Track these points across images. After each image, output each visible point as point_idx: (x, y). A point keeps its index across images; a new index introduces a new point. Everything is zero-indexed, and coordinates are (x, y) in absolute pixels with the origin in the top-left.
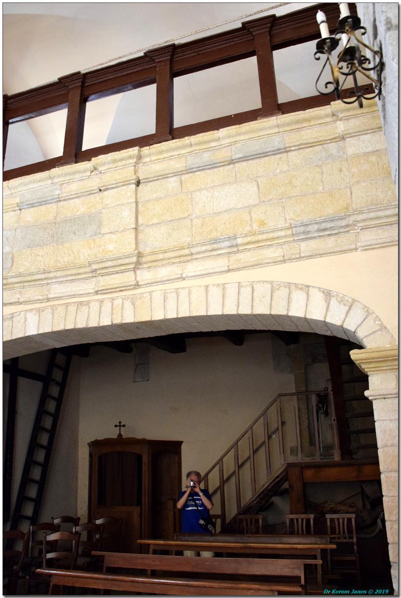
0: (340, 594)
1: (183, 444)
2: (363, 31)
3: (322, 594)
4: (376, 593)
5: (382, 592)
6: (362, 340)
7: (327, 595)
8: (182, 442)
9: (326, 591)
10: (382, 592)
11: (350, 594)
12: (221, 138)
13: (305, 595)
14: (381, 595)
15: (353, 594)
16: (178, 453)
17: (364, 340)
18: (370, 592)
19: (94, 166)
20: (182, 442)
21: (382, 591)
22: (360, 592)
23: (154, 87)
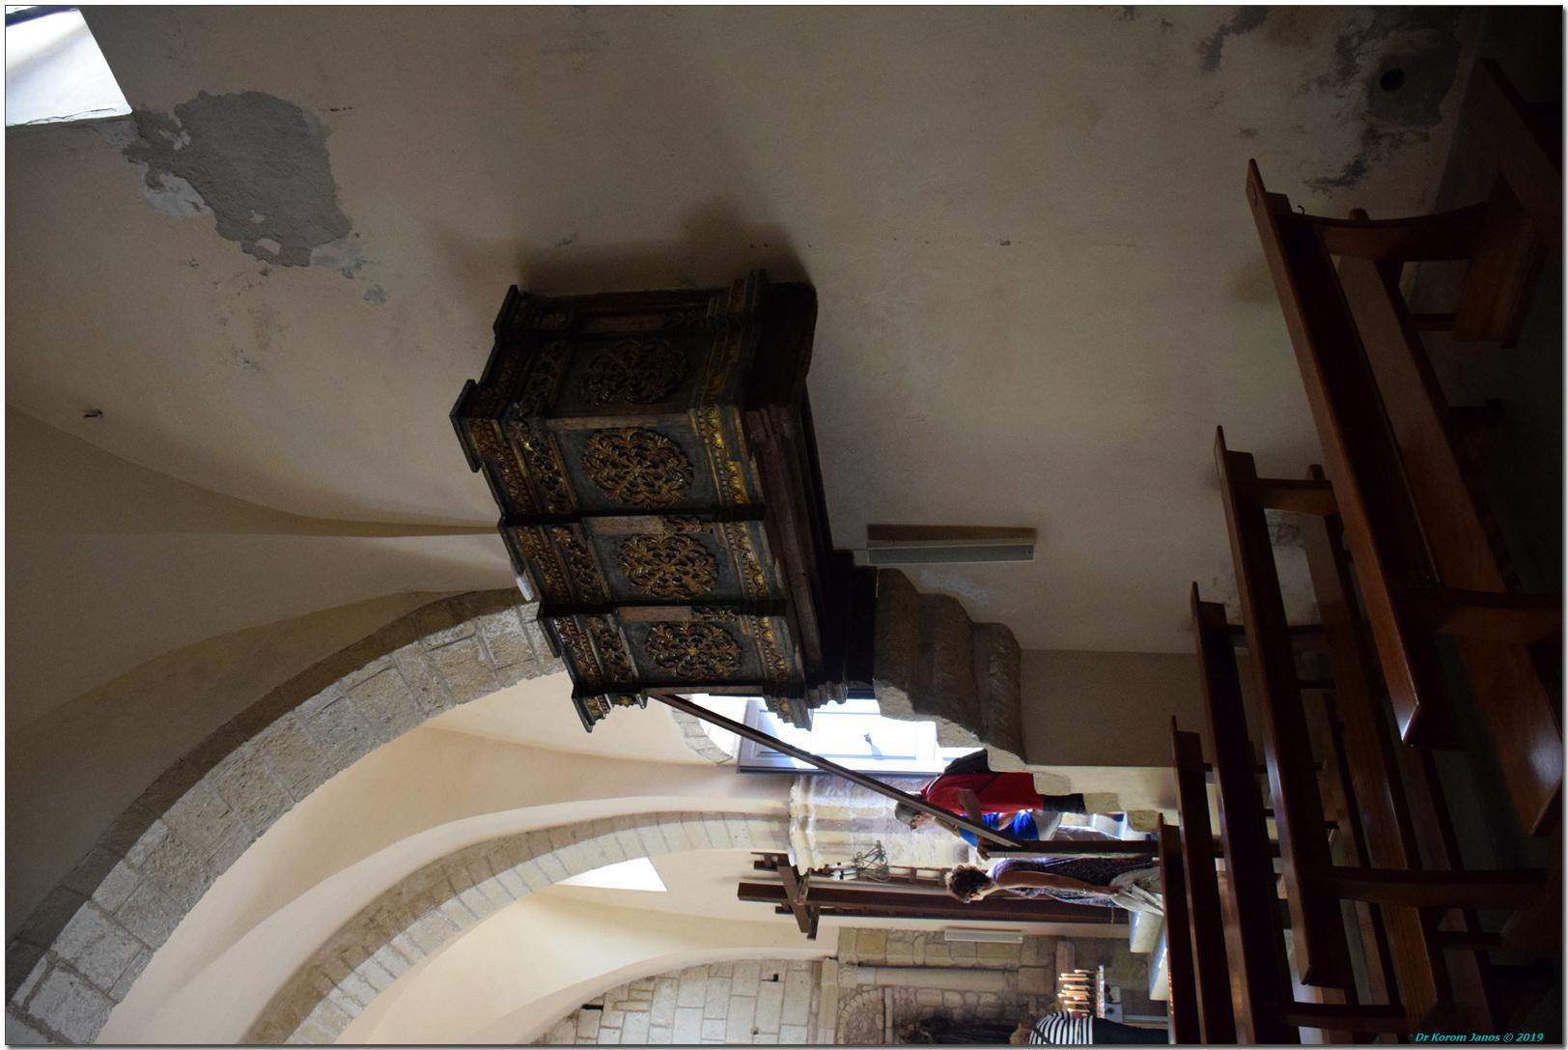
0: (1449, 1043)
1: (805, 730)
4: (1518, 1040)
5: (1531, 1038)
6: (943, 1004)
7: (1422, 1043)
8: (809, 730)
10: (1531, 1038)
11: (1468, 1043)
12: (167, 932)
13: (935, 1043)
14: (1529, 1043)
15: (1474, 1043)
16: (1546, 1042)
18: (1506, 1038)
20: (809, 730)
21: (1531, 1037)
22: (1486, 1038)
23: (1301, 1029)
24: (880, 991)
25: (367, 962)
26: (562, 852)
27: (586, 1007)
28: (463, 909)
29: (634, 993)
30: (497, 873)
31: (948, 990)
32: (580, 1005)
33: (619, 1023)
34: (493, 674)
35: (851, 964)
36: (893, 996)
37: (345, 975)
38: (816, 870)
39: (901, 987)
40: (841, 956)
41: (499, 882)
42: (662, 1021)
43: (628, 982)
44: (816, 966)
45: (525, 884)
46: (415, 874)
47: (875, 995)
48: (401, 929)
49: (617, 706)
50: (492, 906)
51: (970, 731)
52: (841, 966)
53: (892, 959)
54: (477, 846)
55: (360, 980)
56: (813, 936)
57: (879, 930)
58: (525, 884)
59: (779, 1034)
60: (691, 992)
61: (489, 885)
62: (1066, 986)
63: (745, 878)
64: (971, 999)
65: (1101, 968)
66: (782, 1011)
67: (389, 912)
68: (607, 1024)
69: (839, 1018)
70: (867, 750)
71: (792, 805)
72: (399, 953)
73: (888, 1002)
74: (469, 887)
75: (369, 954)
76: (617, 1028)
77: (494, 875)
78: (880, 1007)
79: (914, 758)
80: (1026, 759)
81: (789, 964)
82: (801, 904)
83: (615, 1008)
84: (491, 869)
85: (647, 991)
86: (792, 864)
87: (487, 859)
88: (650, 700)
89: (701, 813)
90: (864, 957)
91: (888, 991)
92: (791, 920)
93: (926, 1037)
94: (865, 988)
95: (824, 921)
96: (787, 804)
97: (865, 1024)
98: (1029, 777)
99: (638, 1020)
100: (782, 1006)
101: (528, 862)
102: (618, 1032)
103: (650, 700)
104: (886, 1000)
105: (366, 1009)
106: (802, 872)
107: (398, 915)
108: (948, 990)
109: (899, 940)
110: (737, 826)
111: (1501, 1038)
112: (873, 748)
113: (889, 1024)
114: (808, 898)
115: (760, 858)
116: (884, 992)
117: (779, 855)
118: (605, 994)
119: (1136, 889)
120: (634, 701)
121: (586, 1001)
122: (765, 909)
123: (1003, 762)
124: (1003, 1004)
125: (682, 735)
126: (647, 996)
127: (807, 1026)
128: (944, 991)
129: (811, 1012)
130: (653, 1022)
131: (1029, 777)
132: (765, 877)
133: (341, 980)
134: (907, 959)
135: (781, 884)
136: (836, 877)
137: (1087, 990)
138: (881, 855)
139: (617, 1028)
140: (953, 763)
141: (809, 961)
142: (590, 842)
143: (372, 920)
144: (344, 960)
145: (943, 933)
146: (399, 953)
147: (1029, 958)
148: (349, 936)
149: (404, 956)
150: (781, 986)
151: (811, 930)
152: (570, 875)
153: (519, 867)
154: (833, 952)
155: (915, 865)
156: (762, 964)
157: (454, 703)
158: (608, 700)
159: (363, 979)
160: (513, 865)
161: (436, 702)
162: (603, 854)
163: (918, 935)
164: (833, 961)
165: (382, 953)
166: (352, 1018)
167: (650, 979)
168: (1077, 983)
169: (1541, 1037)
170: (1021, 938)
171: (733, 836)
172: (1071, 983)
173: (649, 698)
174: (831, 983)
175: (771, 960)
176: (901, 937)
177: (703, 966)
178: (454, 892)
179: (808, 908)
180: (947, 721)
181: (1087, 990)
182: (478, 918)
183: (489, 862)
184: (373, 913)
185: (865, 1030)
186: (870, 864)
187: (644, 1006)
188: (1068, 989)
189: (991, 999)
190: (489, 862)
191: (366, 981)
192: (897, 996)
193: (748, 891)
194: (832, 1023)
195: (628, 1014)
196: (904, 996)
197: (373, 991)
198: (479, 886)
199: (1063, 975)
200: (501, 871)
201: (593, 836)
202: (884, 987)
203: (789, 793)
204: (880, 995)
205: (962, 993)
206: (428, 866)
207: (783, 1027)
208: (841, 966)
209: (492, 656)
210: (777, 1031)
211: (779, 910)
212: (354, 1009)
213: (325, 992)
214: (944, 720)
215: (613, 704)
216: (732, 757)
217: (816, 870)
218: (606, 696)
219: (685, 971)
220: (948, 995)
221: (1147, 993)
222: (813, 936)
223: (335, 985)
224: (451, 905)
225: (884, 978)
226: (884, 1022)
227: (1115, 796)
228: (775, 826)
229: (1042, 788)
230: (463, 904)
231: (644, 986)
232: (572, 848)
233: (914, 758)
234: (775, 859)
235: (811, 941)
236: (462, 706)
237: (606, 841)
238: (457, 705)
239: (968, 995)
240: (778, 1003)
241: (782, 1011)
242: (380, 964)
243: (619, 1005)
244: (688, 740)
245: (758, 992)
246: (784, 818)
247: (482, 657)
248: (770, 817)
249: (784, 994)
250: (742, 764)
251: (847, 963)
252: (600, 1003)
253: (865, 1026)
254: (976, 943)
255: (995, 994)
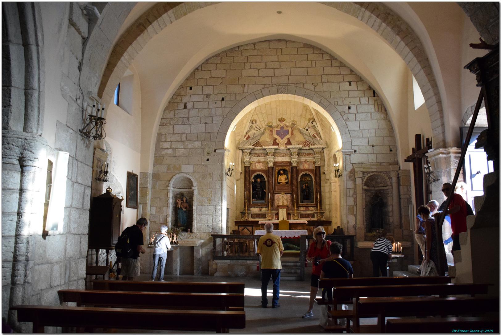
0: (463, 333)
2: (30, 284)
3: (228, 332)
7: (454, 333)
9: (454, 331)
11: (469, 333)
14: (488, 333)
15: (471, 333)
16: (494, 332)
17: (333, 218)
18: (481, 331)
19: (241, 212)
22: (475, 331)
24: (390, 185)
25: (375, 17)
26: (422, 72)
27: (374, 92)
28: (398, 43)
29: (380, 106)
30: (412, 52)
31: (393, 206)
32: (374, 90)
33: (370, 103)
34: (485, 27)
35: (398, 174)
36: (389, 189)
37: (369, 11)
38: (428, 159)
39: (392, 191)
40: (401, 171)
41: (409, 53)
42: (373, 116)
43: (384, 103)
44: (397, 163)
45: (409, 62)
46: (407, 24)
47: (389, 183)
48: (387, 25)
49: (476, 75)
50: (400, 53)
51: (481, 208)
52: (397, 171)
53: (401, 188)
54: (420, 42)
55: (369, 16)
56: (406, 161)
57: (410, 183)
58: (409, 62)
59: (373, 154)
60: (383, 124)
61: (407, 49)
62: (396, 245)
63: (423, 136)
64: (391, 214)
65: (403, 256)
66: (381, 154)
67: (393, 19)
68: (370, 99)
69: (380, 172)
70: (474, 172)
71: (450, 148)
72: (380, 26)
73: (387, 188)
74: (405, 43)
75: (378, 17)
76: (369, 103)
77: (411, 50)
78: (385, 185)
79: (472, 190)
80: (472, 229)
81: (396, 154)
82: (416, 156)
83: (375, 101)
84: (412, 49)
85: (382, 110)
86: (429, 151)
87: (416, 46)
88: (480, 88)
89: (443, 117)
90: (401, 179)
91: (390, 187)
92: (411, 153)
93: (377, 200)
94: (391, 180)
95: (411, 165)
96: (450, 146)
97: (379, 181)
98: (465, 230)
99: (372, 109)
100: (382, 154)
101: (417, 61)
102: (367, 103)
103: (480, 88)
104: (388, 187)
105: (361, 21)
106: (426, 155)
107: (392, 22)
108: (393, 206)
109: (408, 189)
110: (440, 130)
111: (480, 331)
112: (475, 175)
113: (380, 188)
114: (418, 158)
115: (430, 140)
116: (390, 186)
117: (432, 146)
118: (379, 96)
119: (429, 269)
120: (478, 81)
121: (376, 91)
122: (412, 144)
123: (470, 222)
124: (390, 224)
125: (472, 105)
126: (380, 110)
127: (377, 162)
128: (392, 205)
129: (381, 163)
130: (372, 113)
131: (465, 230)
132: (424, 144)
133: (368, 10)
134: (402, 193)
135: (422, 148)
136: (425, 166)
137: (396, 251)
138: (435, 181)
139: (369, 103)
140: (466, 201)
141: (398, 161)
142: (427, 81)
143: (389, 14)
144: (374, 9)
145: (411, 204)
146: (380, 26)
147: (405, 232)
148: (382, 8)
149: (379, 28)
150: (389, 153)
151: (408, 160)
152: (415, 76)
153: (415, 58)
154: (401, 168)
155: (432, 193)
156: (395, 146)
157: (470, 16)
158: (478, 72)
159: (370, 17)
160: (415, 56)
161: (470, 9)
162: (424, 86)
163: (410, 195)
164: (398, 169)
165: (379, 20)
166: (357, 18)
167: (386, 110)
168: (398, 248)
169: (492, 331)
170: (412, 230)
171: (436, 129)
172: (398, 246)
173: (481, 87)
174: (391, 169)
175: (397, 149)
176: (409, 190)
177: (392, 126)
178: (403, 39)
179: (415, 158)
180: (485, 200)
181: (396, 251)
182: (395, 49)
183: (415, 48)
184: (391, 14)
185: (378, 181)
186: (432, 178)
187: (377, 110)
188: (395, 245)
189: (391, 220)
190: (415, 48)
191: (369, 18)
192: (389, 190)
193: (418, 137)
194: (380, 170)
195: (373, 105)
196: (390, 193)
197: (366, 22)
198: (406, 47)
199: (400, 244)
200: (413, 53)
201: (429, 81)
202: (392, 186)
203: (454, 147)
204: (389, 185)
205: (392, 211)
206: (410, 27)
207: (375, 155)
208: (397, 171)
209: (492, 24)
210: (374, 153)
211: (413, 149)
212: (360, 18)
213: (363, 6)
214: (485, 198)
215: (477, 74)
216: (465, 125)
217: (428, 159)
218: (480, 71)
219: (390, 121)
220: (391, 206)
221: (394, 270)
222: (406, 161)
223: (366, 9)
224: (398, 38)
225: (395, 185)
226: (380, 187)
227: (461, 261)
228: (441, 144)
229: (461, 235)
230: (400, 42)
231: (383, 109)
232: (424, 75)
233: (472, 190)
234: (430, 145)
235: (404, 160)
236: (470, 19)
237: (429, 86)
238: (469, 18)
239: (392, 213)
240: (383, 152)
241: (381, 154)
242: (375, 21)
243: (376, 102)
244: (470, 107)
245: (386, 145)
246: (445, 146)
247: (491, 21)
248: (444, 141)
249: (386, 154)
250: (463, 129)
251: (398, 173)
252: (376, 96)
253: (379, 181)
254: (409, 215)
255: (393, 222)
